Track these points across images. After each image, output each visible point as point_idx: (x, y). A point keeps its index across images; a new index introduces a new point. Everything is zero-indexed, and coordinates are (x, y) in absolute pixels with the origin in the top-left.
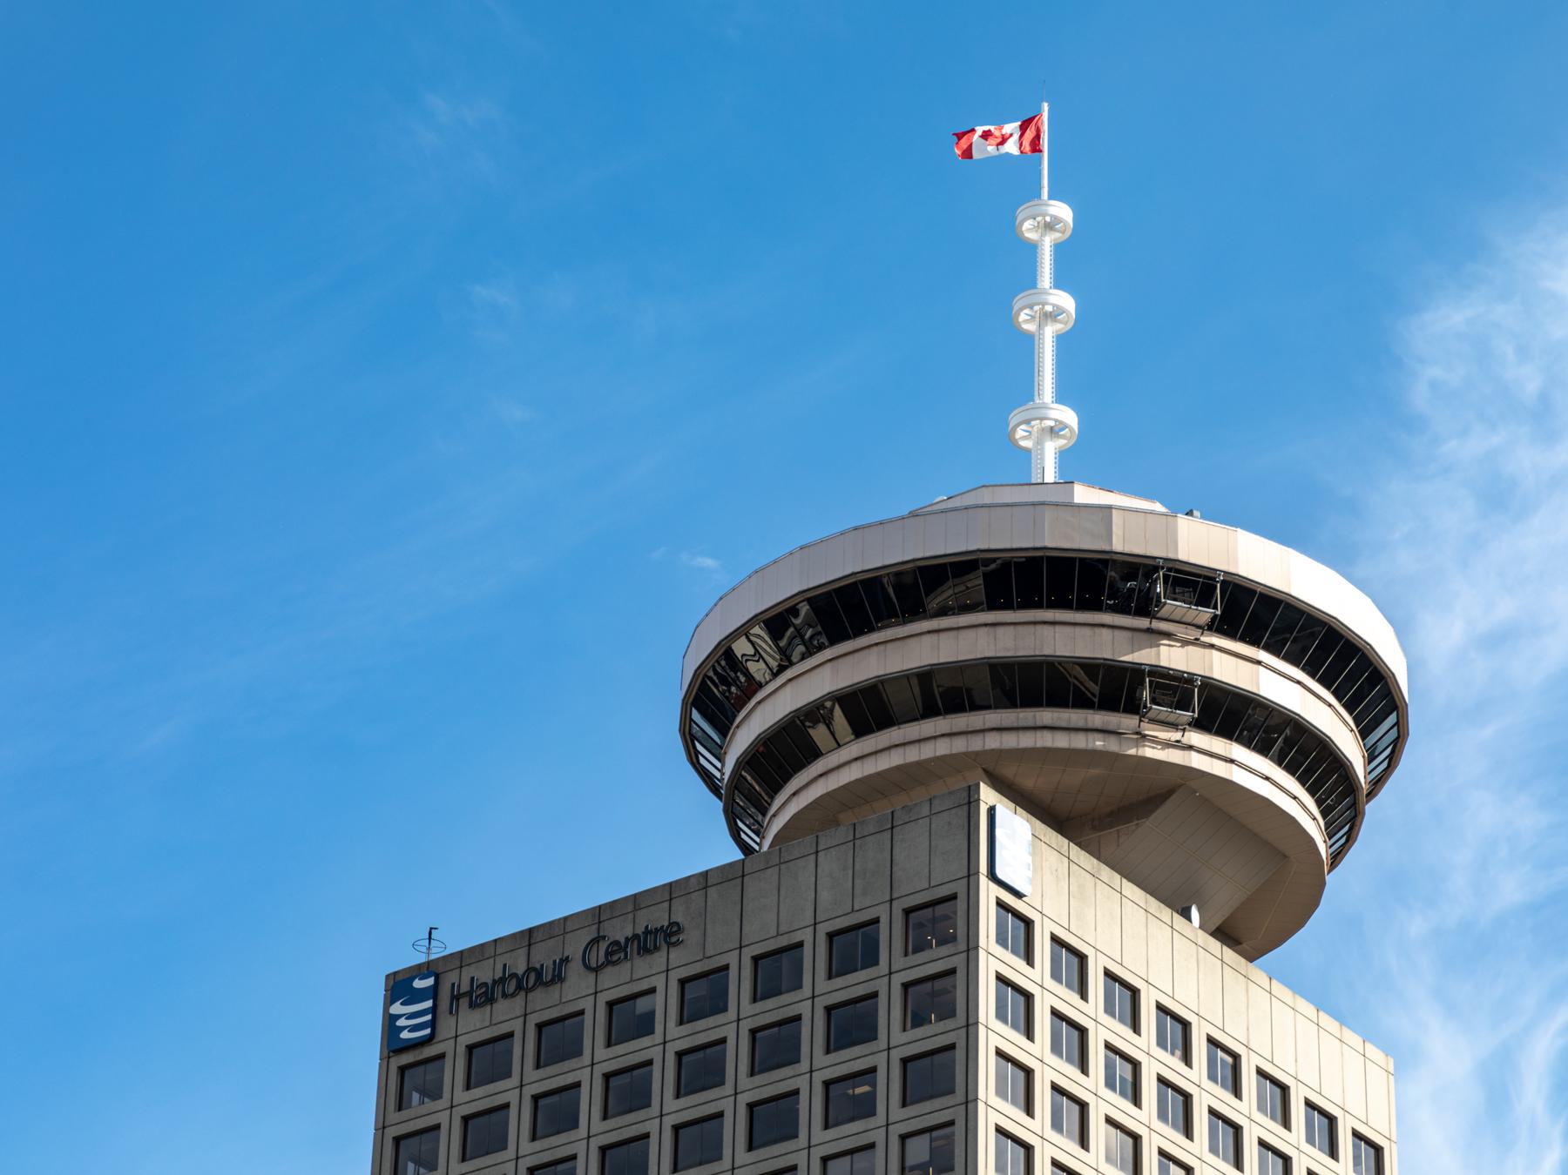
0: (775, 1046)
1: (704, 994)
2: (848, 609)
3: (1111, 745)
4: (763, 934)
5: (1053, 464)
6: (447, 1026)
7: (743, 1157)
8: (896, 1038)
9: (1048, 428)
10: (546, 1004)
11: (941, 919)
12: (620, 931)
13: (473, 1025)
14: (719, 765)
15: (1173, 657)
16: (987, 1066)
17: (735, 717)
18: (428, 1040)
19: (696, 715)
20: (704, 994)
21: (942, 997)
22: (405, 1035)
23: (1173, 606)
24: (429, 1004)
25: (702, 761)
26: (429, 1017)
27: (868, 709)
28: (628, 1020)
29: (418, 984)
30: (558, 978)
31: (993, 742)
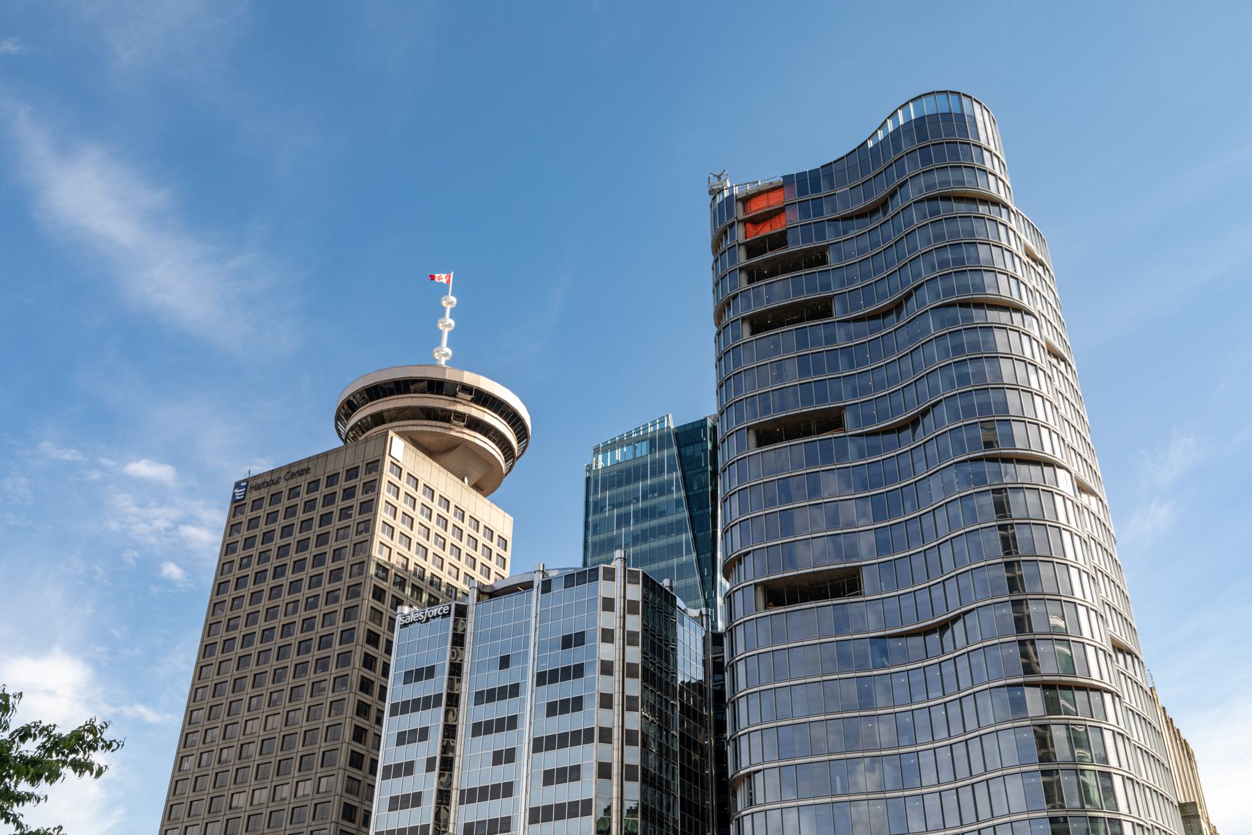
0: (330, 499)
1: (313, 486)
2: (375, 392)
3: (442, 431)
4: (330, 470)
5: (441, 359)
6: (248, 495)
8: (360, 497)
9: (444, 353)
10: (274, 489)
11: (375, 466)
12: (294, 470)
13: (255, 495)
15: (460, 408)
16: (382, 504)
20: (313, 486)
21: (372, 486)
23: (461, 394)
28: (293, 492)
30: (277, 482)
31: (410, 428)
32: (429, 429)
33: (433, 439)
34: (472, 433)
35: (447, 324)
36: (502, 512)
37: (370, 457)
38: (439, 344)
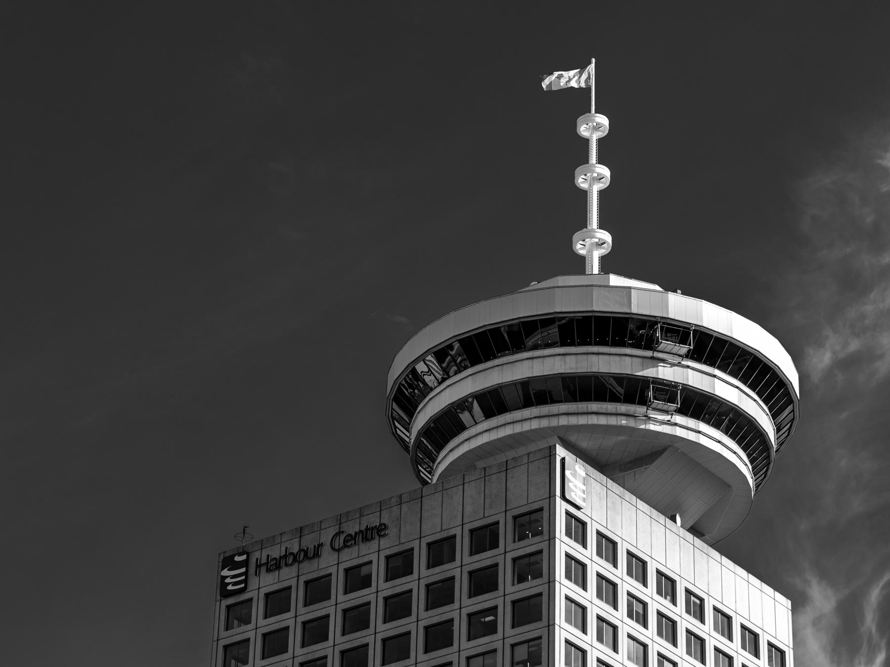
0: (441, 594)
6: (253, 583)
8: (510, 590)
10: (311, 570)
11: (534, 522)
15: (665, 373)
22: (230, 587)
23: (665, 345)
28: (357, 579)
29: (237, 559)
30: (317, 554)
31: (564, 421)
32: (602, 421)
33: (611, 441)
34: (691, 422)
35: (595, 177)
36: (742, 572)
37: (520, 503)
38: (583, 223)
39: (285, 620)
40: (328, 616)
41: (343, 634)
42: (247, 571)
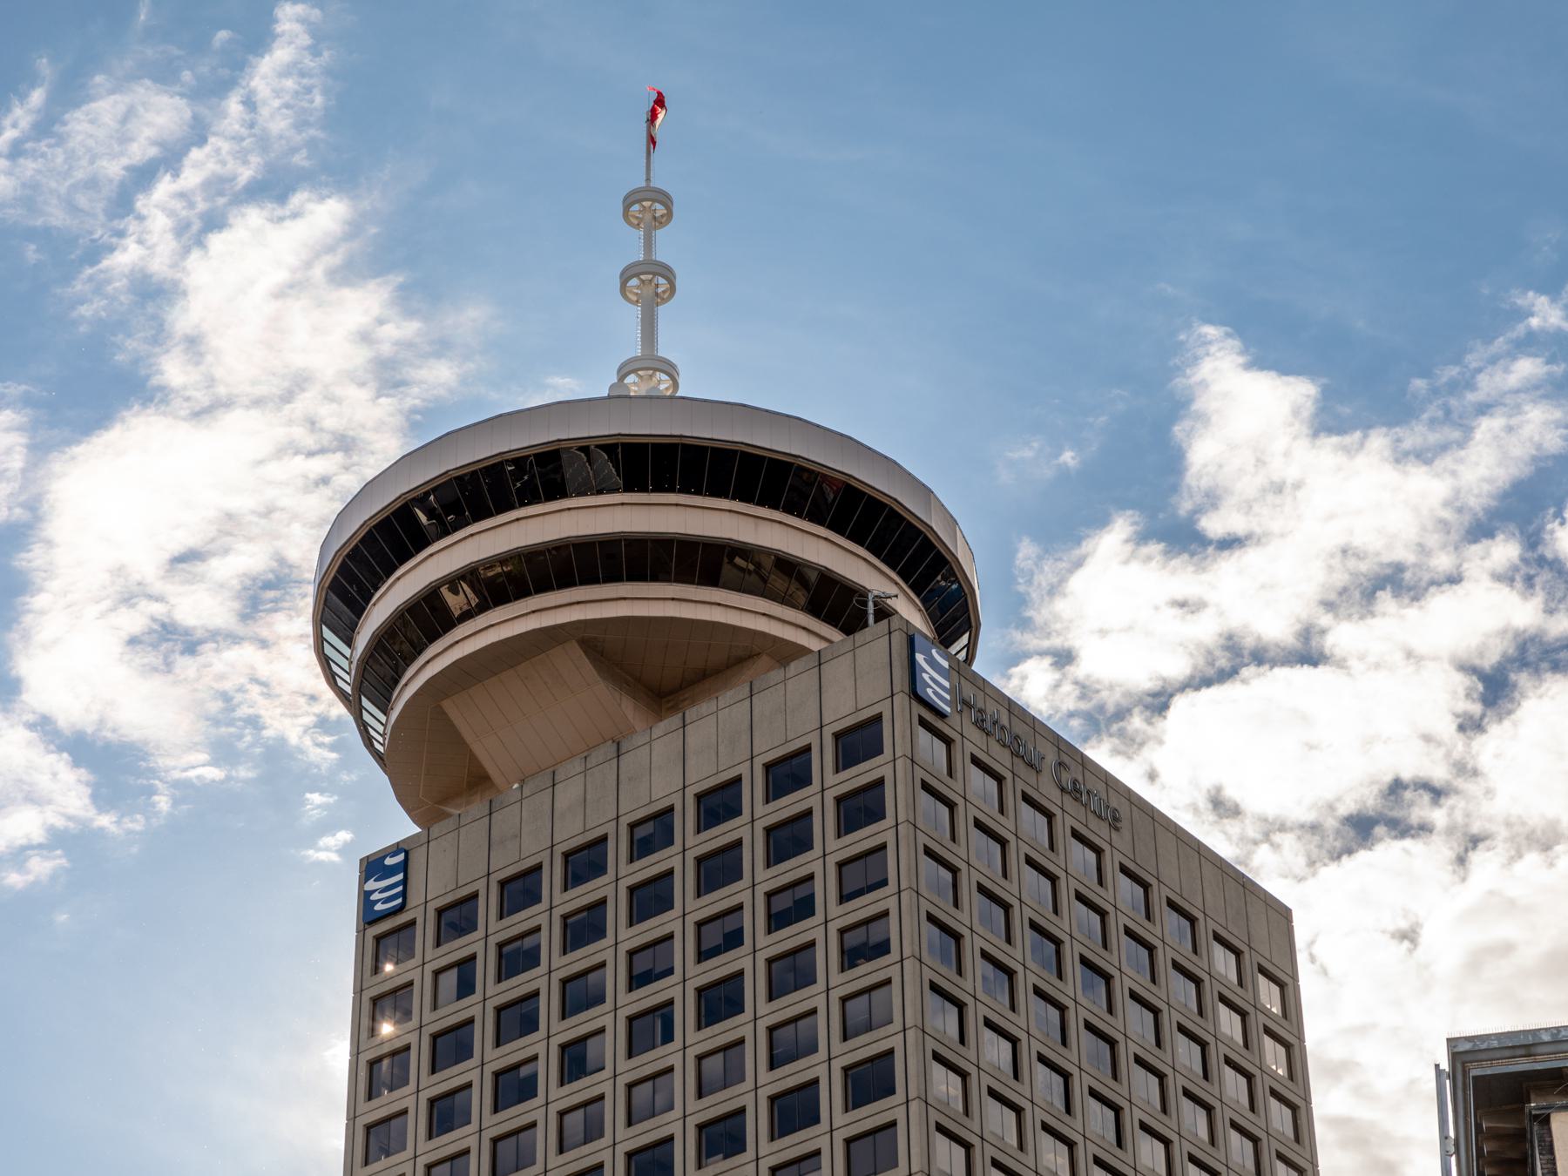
7: (554, 1160)
14: (383, 718)
17: (372, 595)
18: (401, 909)
19: (326, 631)
22: (379, 907)
24: (400, 877)
25: (366, 716)
26: (400, 888)
27: (498, 584)
29: (389, 861)
39: (633, 936)
40: (741, 973)
41: (430, 1137)
42: (405, 882)
